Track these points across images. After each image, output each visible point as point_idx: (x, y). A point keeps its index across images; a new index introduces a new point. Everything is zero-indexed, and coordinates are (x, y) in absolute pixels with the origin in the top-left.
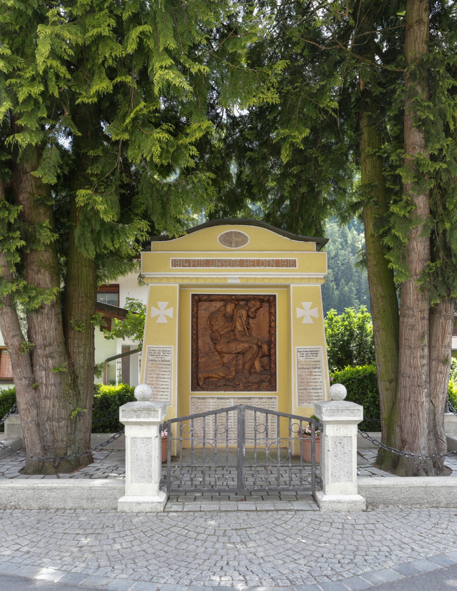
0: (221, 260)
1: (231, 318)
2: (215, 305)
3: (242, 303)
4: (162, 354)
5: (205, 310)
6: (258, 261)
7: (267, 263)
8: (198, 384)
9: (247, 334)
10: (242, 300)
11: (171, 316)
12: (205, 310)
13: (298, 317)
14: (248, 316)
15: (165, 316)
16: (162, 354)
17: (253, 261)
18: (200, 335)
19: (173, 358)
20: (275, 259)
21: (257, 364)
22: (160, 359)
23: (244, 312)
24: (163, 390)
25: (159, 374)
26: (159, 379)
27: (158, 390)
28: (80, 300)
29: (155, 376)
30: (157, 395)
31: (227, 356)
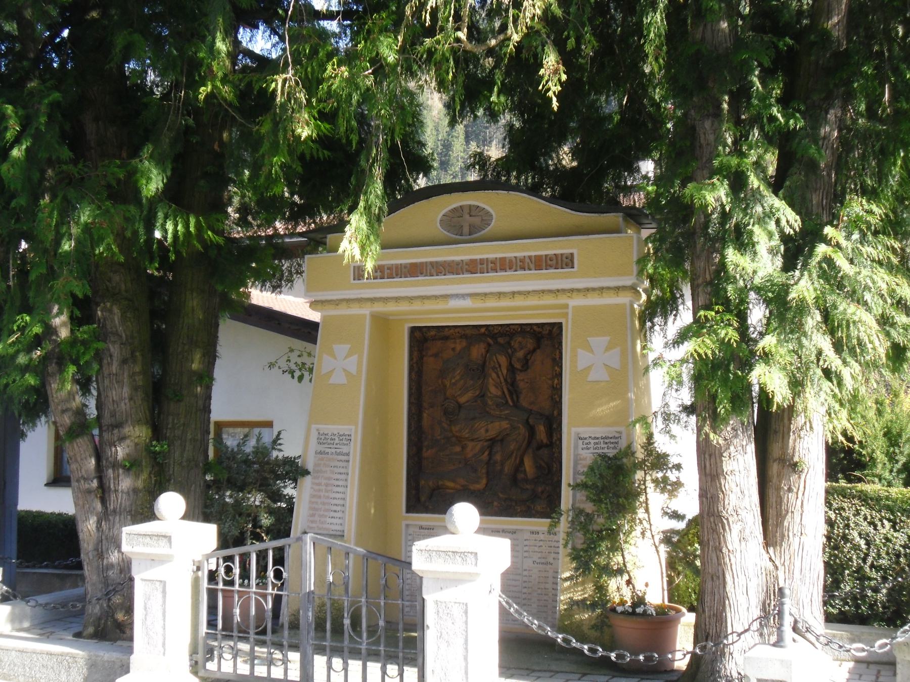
0: (437, 262)
1: (480, 371)
2: (452, 346)
3: (501, 340)
4: (337, 441)
5: (436, 355)
6: (503, 260)
7: (519, 263)
8: (418, 500)
9: (510, 401)
10: (502, 335)
11: (353, 370)
12: (436, 355)
13: (579, 369)
14: (511, 369)
15: (345, 370)
16: (337, 441)
17: (494, 262)
18: (425, 405)
19: (355, 450)
20: (533, 253)
21: (528, 464)
22: (334, 451)
23: (503, 360)
24: (335, 508)
25: (329, 479)
26: (329, 488)
27: (327, 507)
28: (180, 349)
29: (324, 482)
30: (326, 516)
31: (470, 445)
